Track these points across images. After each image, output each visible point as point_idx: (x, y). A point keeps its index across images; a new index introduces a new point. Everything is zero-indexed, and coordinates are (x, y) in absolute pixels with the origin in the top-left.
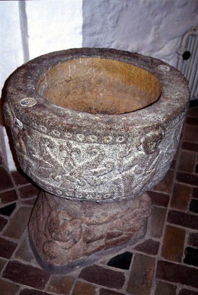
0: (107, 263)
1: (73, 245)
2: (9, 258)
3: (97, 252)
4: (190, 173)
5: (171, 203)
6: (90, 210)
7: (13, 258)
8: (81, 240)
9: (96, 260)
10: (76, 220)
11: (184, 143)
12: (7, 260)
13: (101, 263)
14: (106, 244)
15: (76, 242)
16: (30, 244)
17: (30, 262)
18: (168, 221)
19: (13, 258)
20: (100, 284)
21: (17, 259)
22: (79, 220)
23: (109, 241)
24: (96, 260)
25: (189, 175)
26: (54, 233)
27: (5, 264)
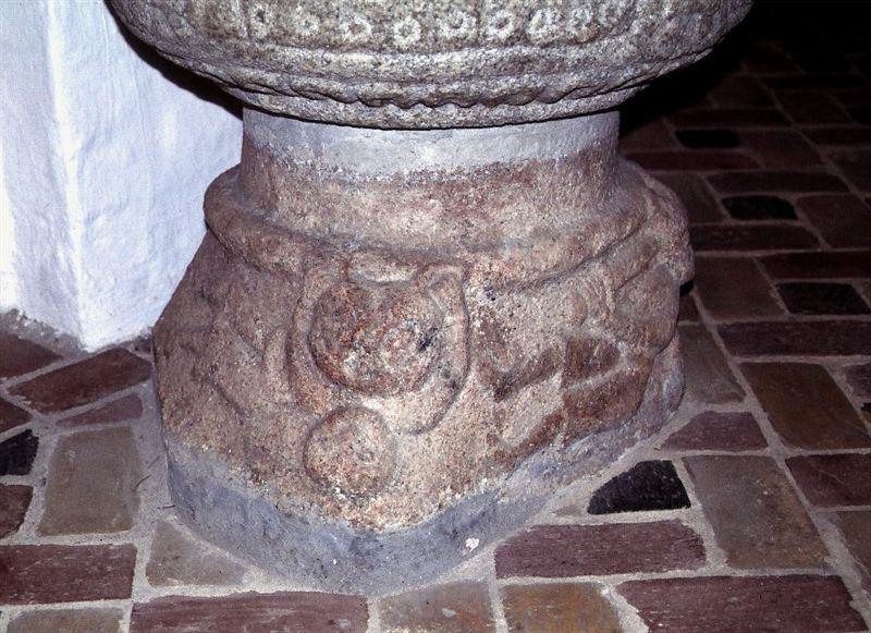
0: (585, 509)
1: (448, 403)
2: (128, 595)
3: (534, 459)
4: (716, 224)
5: (707, 306)
6: (484, 216)
7: (144, 591)
8: (472, 376)
9: (535, 504)
10: (441, 271)
11: (499, 555)
12: (125, 606)
13: (560, 513)
14: (567, 401)
15: (455, 387)
16: (309, 48)
17: (239, 583)
18: (734, 353)
19: (144, 591)
20: (608, 571)
21: (164, 592)
22: (451, 269)
23: (575, 386)
24: (535, 504)
25: (714, 228)
26: (352, 356)
27: (121, 617)
